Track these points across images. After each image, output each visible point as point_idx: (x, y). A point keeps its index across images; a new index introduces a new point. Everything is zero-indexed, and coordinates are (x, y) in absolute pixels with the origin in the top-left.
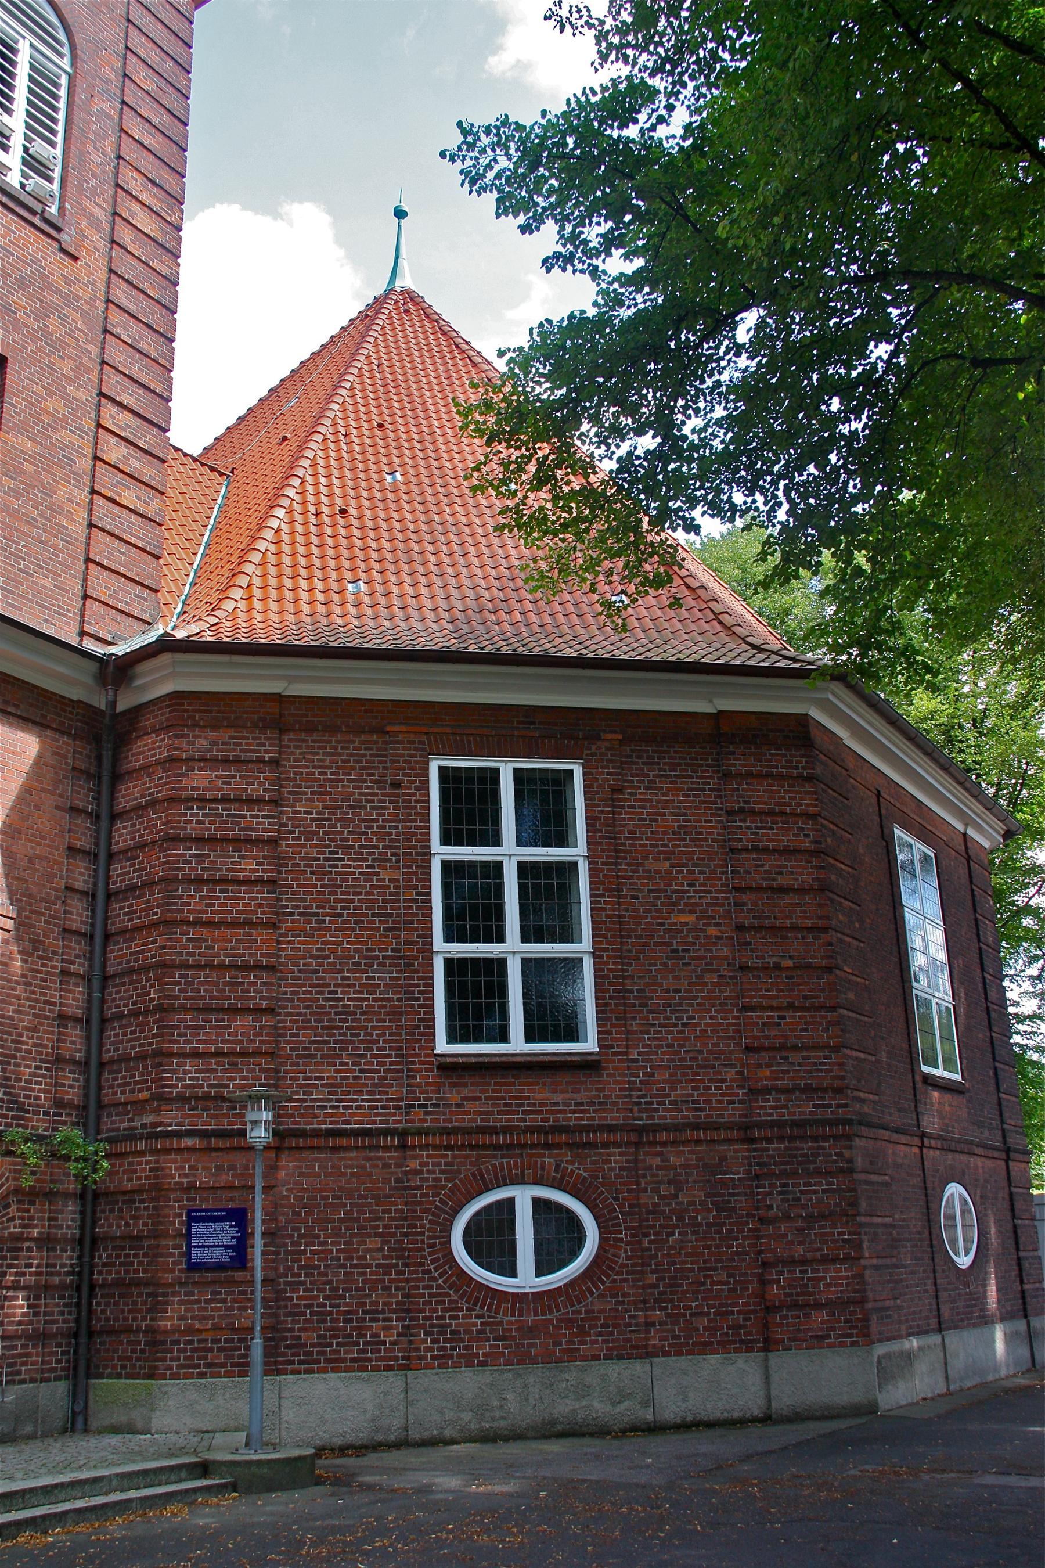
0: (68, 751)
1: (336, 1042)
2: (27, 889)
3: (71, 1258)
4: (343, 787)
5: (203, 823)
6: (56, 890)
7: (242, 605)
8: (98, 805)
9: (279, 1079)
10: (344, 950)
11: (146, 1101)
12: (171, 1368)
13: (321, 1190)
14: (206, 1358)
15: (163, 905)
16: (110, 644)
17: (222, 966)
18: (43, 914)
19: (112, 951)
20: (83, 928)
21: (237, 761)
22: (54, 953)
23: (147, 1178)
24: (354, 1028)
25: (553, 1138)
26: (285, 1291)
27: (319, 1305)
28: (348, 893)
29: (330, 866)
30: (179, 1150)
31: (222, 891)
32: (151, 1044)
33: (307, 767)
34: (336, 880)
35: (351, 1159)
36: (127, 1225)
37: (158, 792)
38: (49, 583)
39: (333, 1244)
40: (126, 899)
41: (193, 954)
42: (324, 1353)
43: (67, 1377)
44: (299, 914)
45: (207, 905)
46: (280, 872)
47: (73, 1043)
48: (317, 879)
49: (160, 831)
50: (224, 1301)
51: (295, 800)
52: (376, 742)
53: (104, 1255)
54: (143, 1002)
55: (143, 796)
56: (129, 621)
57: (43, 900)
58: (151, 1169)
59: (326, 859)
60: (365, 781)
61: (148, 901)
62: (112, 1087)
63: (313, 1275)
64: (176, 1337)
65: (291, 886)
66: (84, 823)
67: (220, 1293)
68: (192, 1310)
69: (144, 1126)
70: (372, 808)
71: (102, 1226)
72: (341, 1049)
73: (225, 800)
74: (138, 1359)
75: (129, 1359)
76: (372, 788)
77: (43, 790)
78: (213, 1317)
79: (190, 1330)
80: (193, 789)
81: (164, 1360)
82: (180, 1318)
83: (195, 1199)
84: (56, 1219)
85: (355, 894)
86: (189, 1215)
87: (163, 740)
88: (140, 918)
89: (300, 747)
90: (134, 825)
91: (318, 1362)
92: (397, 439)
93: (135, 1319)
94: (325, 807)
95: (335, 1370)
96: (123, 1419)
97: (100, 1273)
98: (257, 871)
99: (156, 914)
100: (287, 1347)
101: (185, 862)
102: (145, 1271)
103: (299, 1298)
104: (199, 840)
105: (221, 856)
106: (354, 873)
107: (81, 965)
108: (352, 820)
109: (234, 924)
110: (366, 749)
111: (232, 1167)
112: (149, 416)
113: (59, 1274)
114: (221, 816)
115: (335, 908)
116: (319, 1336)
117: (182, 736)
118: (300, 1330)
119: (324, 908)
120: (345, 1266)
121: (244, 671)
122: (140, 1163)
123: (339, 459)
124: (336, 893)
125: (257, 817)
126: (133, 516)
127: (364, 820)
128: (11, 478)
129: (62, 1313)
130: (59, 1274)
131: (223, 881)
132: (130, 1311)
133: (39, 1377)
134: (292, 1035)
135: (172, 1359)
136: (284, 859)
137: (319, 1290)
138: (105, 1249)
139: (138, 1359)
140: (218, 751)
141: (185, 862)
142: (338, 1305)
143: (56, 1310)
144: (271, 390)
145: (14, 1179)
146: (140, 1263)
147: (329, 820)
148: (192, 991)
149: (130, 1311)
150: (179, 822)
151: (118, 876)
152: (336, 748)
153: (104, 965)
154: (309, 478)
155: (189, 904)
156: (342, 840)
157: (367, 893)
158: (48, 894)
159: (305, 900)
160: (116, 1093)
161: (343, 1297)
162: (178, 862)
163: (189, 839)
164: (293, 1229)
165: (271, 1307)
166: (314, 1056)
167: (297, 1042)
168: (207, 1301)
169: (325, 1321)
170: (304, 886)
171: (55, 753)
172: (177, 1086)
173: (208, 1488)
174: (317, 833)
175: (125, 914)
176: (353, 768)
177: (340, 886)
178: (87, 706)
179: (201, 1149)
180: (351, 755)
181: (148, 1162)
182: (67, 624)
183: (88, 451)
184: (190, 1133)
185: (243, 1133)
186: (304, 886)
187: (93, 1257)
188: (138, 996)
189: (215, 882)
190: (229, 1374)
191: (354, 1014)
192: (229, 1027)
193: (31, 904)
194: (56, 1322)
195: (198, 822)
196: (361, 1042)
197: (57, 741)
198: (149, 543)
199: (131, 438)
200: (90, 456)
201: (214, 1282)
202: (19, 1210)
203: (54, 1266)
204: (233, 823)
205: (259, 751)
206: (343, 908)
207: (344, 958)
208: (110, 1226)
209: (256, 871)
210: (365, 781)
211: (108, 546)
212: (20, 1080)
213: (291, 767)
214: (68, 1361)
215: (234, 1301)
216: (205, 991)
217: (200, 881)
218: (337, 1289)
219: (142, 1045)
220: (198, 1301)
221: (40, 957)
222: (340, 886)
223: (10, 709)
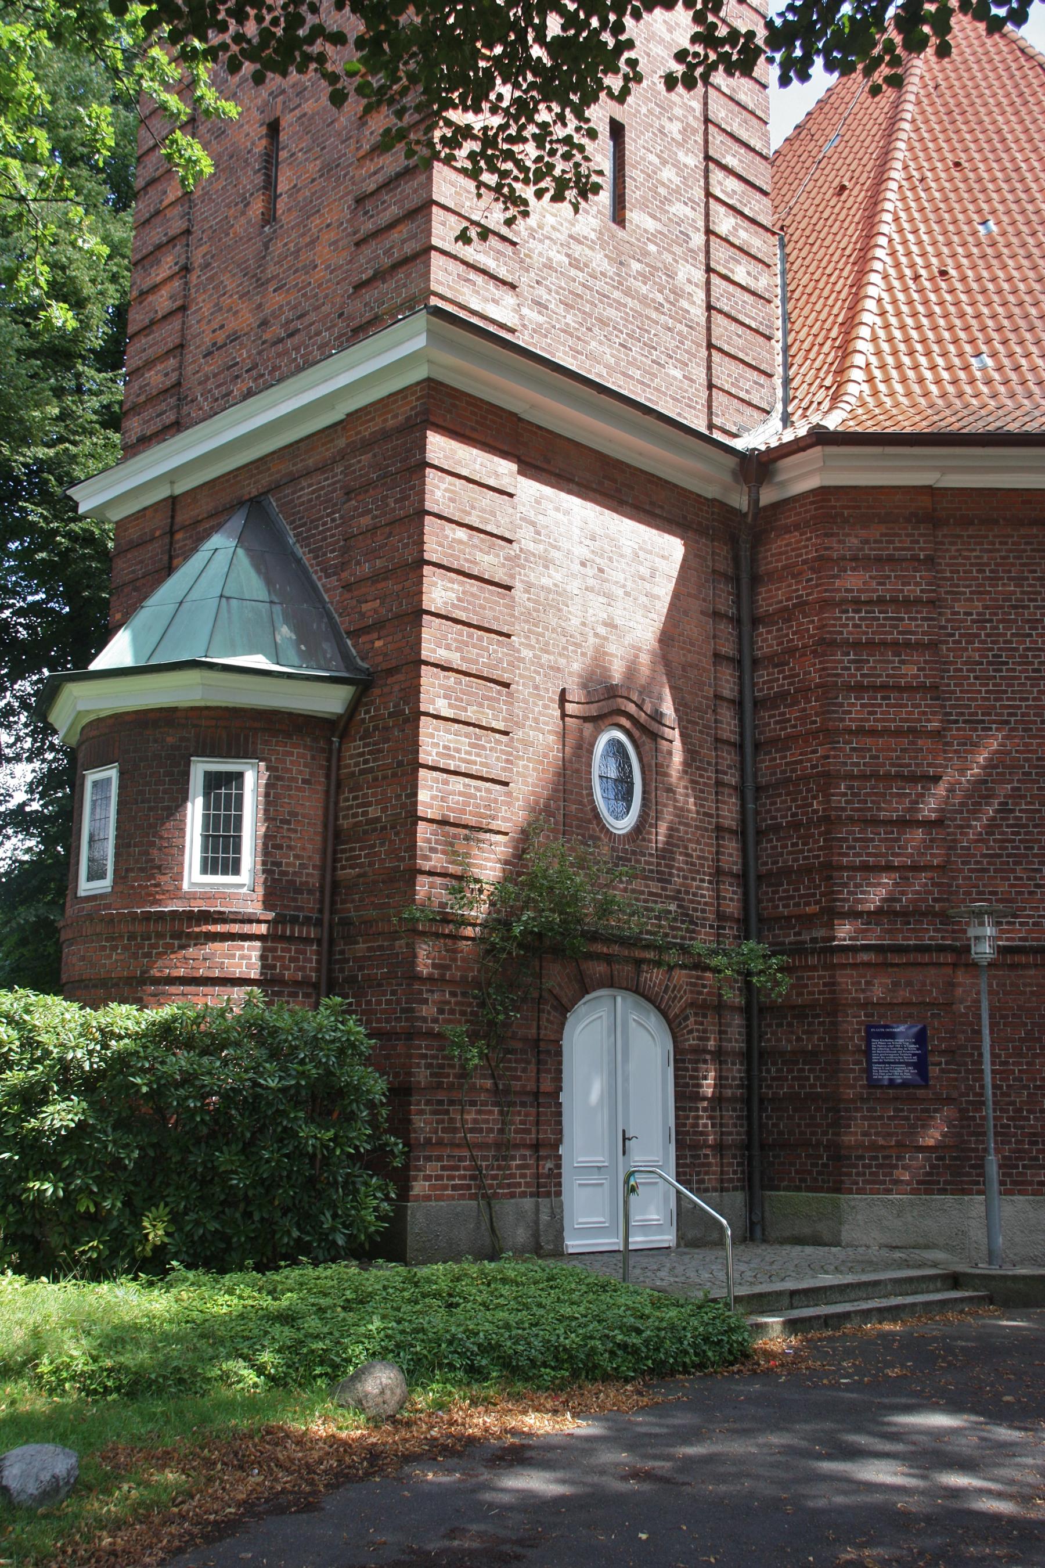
1: (1009, 856)
3: (739, 1071)
4: (1004, 585)
5: (859, 626)
6: (707, 698)
7: (865, 387)
9: (951, 893)
10: (1013, 759)
11: (815, 915)
12: (857, 1183)
15: (823, 713)
16: (735, 436)
17: (887, 777)
18: (697, 724)
19: (764, 761)
21: (890, 559)
23: (820, 993)
25: (938, 958)
26: (968, 1111)
28: (1014, 699)
29: (995, 670)
30: (854, 966)
31: (883, 698)
32: (818, 857)
33: (964, 565)
34: (1000, 685)
35: (1031, 977)
36: (799, 1039)
37: (808, 595)
38: (678, 374)
39: (1014, 1063)
40: (778, 707)
41: (858, 764)
43: (743, 1188)
44: (965, 722)
45: (869, 713)
46: (942, 678)
47: (730, 855)
48: (981, 685)
49: (813, 636)
50: (907, 1118)
51: (954, 600)
52: (1037, 536)
53: (773, 1069)
54: (806, 813)
55: (789, 599)
56: (749, 411)
57: (697, 709)
58: (825, 985)
59: (989, 663)
60: (1027, 579)
61: (804, 710)
62: (772, 900)
64: (860, 1152)
65: (954, 692)
66: (726, 629)
67: (902, 1110)
68: (876, 1126)
69: (814, 940)
70: (1036, 607)
71: (769, 1040)
72: (1015, 863)
73: (881, 601)
74: (819, 1173)
75: (810, 1172)
76: (1034, 586)
77: (689, 595)
78: (897, 1135)
79: (874, 1147)
80: (847, 591)
81: (850, 1174)
82: (865, 1134)
83: (872, 1015)
84: (726, 1032)
85: (1021, 699)
86: (867, 1031)
87: (809, 539)
88: (794, 726)
89: (954, 544)
90: (779, 630)
92: (980, 180)
93: (813, 1133)
94: (986, 607)
95: (1021, 1193)
96: (807, 1231)
97: (769, 1087)
98: (918, 676)
99: (815, 722)
101: (843, 669)
102: (822, 1086)
104: (857, 645)
105: (880, 661)
106: (1019, 678)
107: (733, 775)
108: (1015, 621)
109: (898, 733)
110: (1026, 543)
111: (909, 983)
112: (751, 179)
113: (731, 1087)
114: (878, 619)
115: (1002, 714)
117: (832, 535)
119: (989, 714)
121: (909, 463)
122: (809, 978)
123: (922, 210)
124: (1001, 699)
125: (916, 619)
126: (746, 294)
127: (1028, 621)
128: (638, 260)
129: (735, 1125)
130: (731, 1087)
131: (884, 687)
132: (807, 1126)
135: (858, 1174)
136: (945, 663)
138: (774, 1064)
139: (819, 1173)
140: (871, 549)
141: (843, 669)
142: (1023, 1127)
144: (797, 127)
145: (691, 992)
146: (816, 1078)
147: (990, 621)
148: (859, 802)
149: (807, 1126)
150: (834, 626)
151: (764, 683)
153: (755, 776)
154: (895, 236)
155: (850, 712)
156: (1005, 642)
157: (1034, 699)
159: (969, 707)
160: (778, 906)
161: (1027, 1119)
162: (836, 668)
163: (846, 642)
165: (954, 1126)
166: (987, 870)
167: (967, 856)
168: (889, 1118)
170: (968, 692)
171: (696, 556)
173: (971, 1299)
174: (978, 635)
175: (776, 723)
176: (1013, 565)
177: (1006, 692)
178: (722, 505)
179: (876, 964)
180: (1011, 551)
181: (820, 977)
182: (697, 417)
183: (701, 224)
185: (967, 949)
186: (968, 692)
187: (760, 1071)
188: (798, 807)
189: (875, 688)
191: (1026, 826)
192: (898, 840)
194: (730, 1134)
195: (855, 626)
196: (1035, 855)
198: (761, 323)
199: (738, 206)
200: (703, 229)
201: (896, 1099)
202: (696, 1022)
204: (891, 626)
205: (913, 549)
206: (1010, 715)
207: (1014, 767)
208: (779, 1040)
209: (918, 676)
210: (1027, 579)
211: (726, 329)
213: (947, 565)
214: (743, 1172)
216: (872, 802)
217: (859, 688)
218: (1020, 1110)
219: (805, 858)
220: (881, 1118)
221: (698, 768)
222: (1006, 692)
223: (658, 511)
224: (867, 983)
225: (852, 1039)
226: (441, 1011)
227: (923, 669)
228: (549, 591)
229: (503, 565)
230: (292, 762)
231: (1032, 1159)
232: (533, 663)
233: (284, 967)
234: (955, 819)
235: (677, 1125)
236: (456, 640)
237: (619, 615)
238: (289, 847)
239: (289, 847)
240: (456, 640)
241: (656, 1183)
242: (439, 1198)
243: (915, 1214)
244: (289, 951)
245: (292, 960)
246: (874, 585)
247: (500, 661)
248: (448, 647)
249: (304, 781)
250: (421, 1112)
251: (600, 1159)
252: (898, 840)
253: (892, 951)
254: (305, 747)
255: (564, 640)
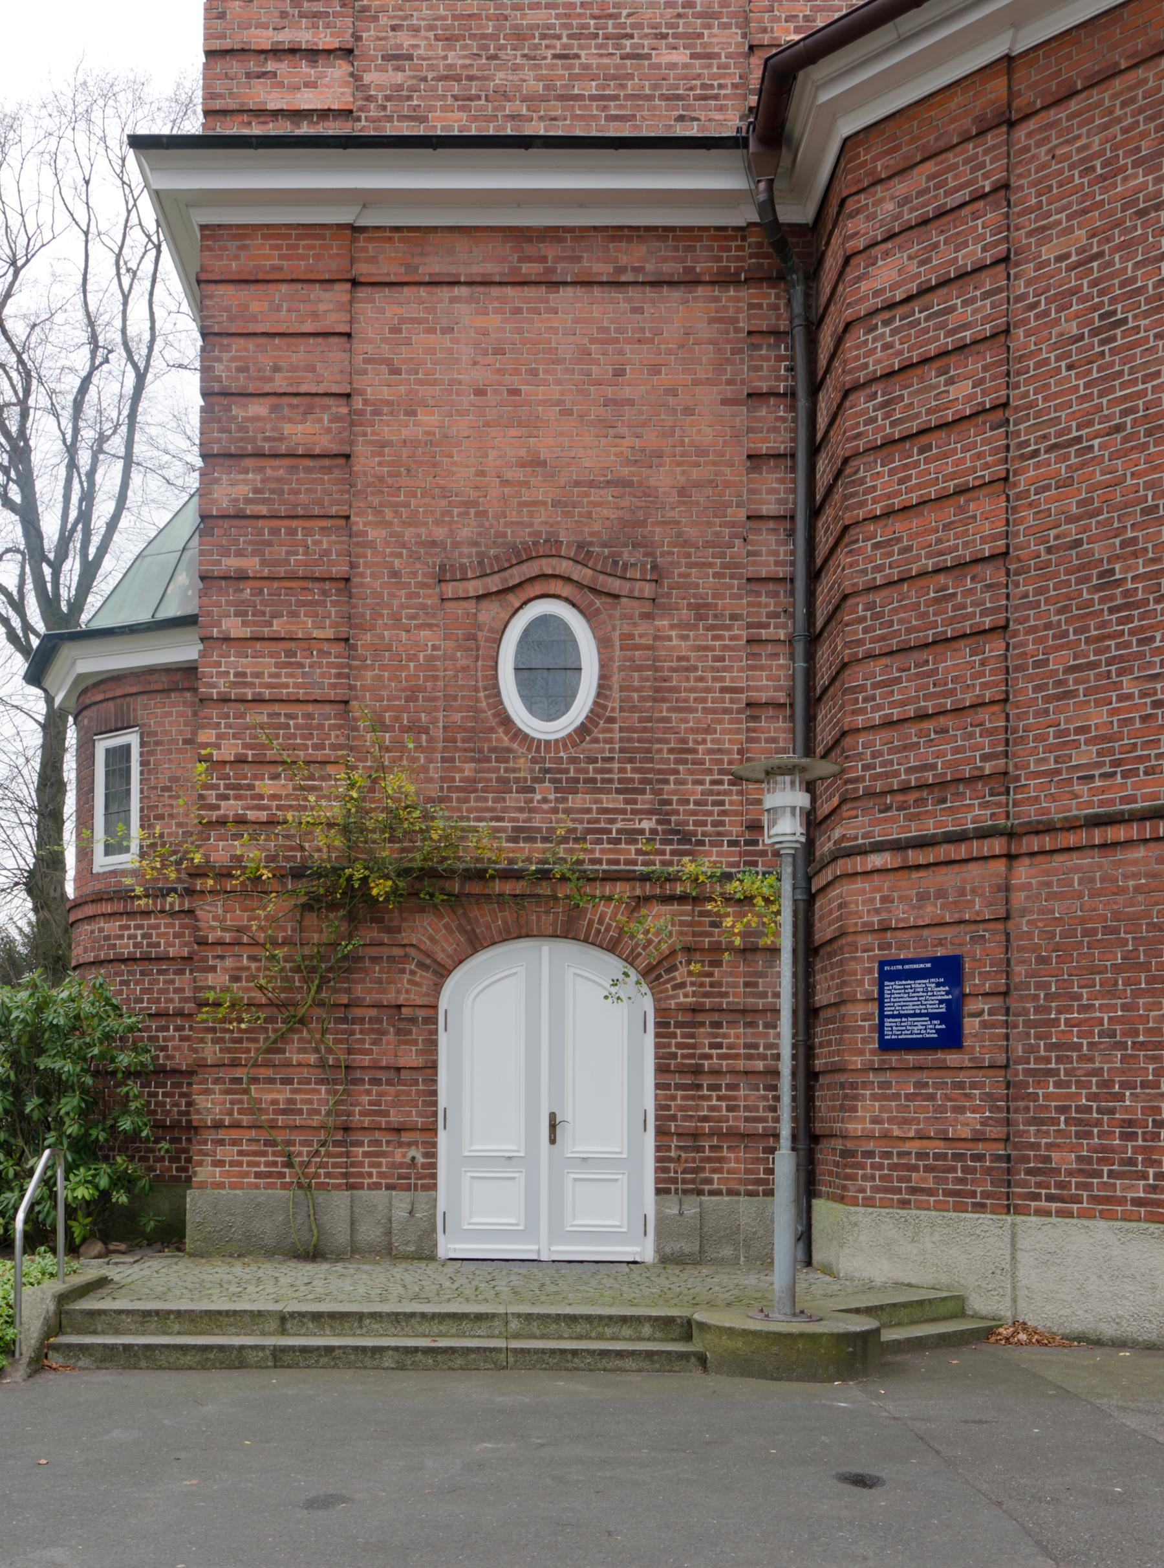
0: (739, 310)
2: (679, 535)
8: (793, 377)
13: (1083, 921)
14: (909, 1180)
18: (711, 565)
20: (781, 572)
22: (734, 617)
24: (1142, 629)
26: (1026, 1085)
27: (1079, 1109)
35: (1135, 862)
39: (1102, 1008)
42: (1086, 1186)
47: (774, 740)
50: (932, 1097)
51: (1039, 244)
57: (708, 544)
63: (1069, 1060)
66: (774, 414)
81: (853, 1178)
82: (875, 1120)
91: (1077, 1200)
100: (1029, 1172)
103: (1047, 1097)
111: (941, 894)
116: (1080, 1159)
118: (1049, 1146)
119: (1090, 423)
120: (1124, 1046)
133: (742, 1188)
134: (1037, 665)
135: (865, 1178)
137: (1079, 1084)
142: (1112, 1111)
143: (762, 1104)
152: (1111, 111)
158: (717, 534)
161: (1120, 1097)
164: (1038, 986)
168: (908, 1097)
169: (1089, 1135)
172: (863, 779)
182: (721, 109)
184: (878, 848)
190: (940, 1207)
193: (688, 555)
197: (717, 299)
203: (755, 1046)
212: (687, 802)
215: (947, 1098)
218: (1108, 1084)
220: (896, 1097)
224: (884, 899)
225: (861, 982)
226: (236, 979)
227: (982, 381)
228: (415, 443)
229: (329, 430)
230: (170, 723)
231: (1123, 1162)
232: (387, 544)
233: (168, 944)
234: (1027, 619)
235: (659, 1107)
236: (251, 542)
237: (545, 446)
238: (171, 816)
239: (171, 816)
240: (251, 542)
241: (616, 1180)
242: (233, 1186)
243: (937, 1237)
244: (173, 926)
245: (176, 935)
246: (913, 268)
247: (327, 552)
248: (240, 553)
249: (186, 742)
250: (207, 1092)
251: (513, 1146)
252: (935, 672)
253: (914, 847)
254: (185, 704)
255: (444, 503)
